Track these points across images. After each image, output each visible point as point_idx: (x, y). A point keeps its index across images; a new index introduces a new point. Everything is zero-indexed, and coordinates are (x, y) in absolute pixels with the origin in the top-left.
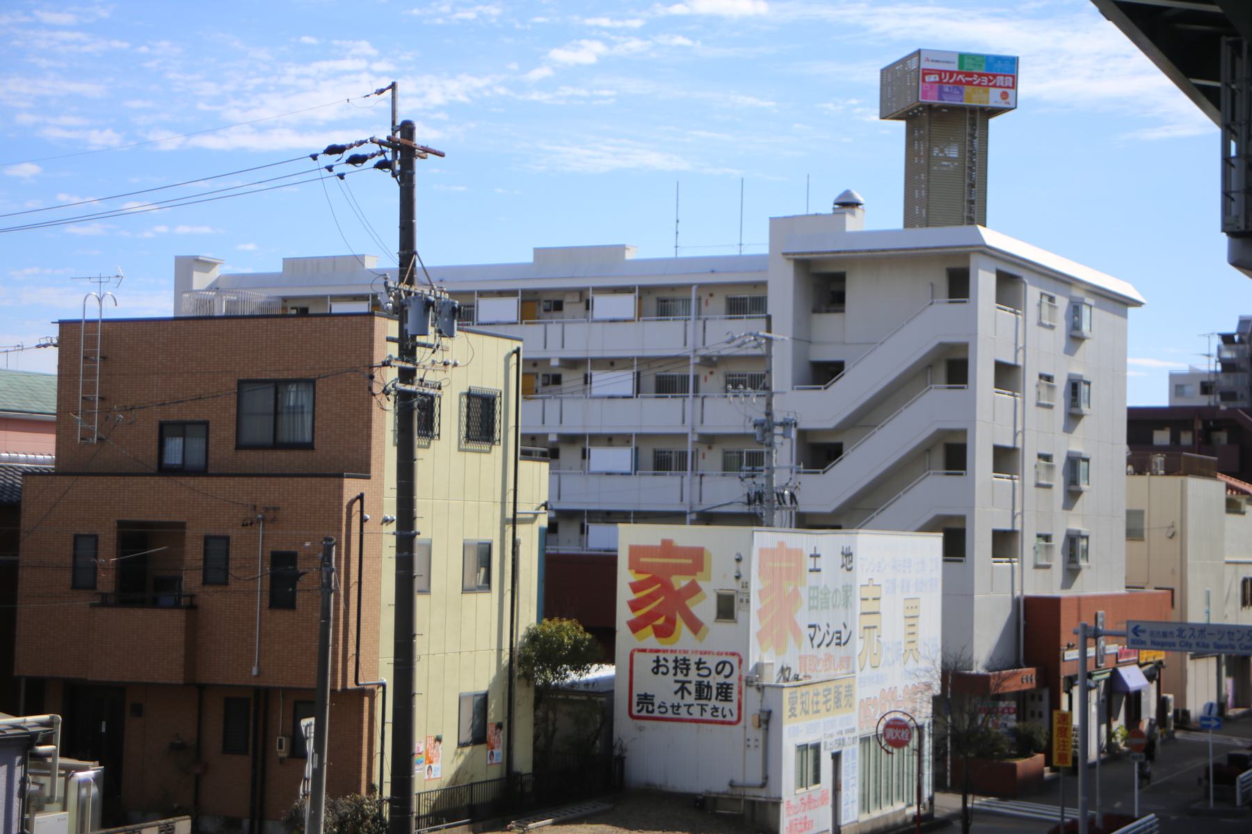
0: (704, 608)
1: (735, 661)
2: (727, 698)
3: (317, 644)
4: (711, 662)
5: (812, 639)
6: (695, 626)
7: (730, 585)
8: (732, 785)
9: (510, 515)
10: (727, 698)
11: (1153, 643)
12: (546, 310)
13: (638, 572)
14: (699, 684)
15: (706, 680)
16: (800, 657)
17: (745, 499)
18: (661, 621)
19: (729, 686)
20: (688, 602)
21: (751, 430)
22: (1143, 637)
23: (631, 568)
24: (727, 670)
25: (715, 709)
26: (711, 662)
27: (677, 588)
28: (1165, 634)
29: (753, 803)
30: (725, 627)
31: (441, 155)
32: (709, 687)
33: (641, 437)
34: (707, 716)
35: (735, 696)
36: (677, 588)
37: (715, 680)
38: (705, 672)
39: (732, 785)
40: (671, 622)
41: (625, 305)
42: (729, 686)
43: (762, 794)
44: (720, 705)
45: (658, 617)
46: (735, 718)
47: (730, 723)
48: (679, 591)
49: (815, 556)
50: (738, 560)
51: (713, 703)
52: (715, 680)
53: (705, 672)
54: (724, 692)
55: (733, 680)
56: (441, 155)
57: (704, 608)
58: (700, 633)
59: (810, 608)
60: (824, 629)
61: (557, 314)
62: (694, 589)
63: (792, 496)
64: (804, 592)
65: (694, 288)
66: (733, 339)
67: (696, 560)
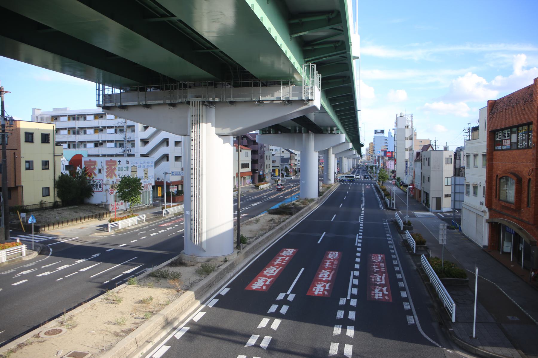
0: (96, 171)
1: (101, 180)
2: (101, 187)
3: (516, 173)
4: (98, 181)
5: (119, 176)
6: (95, 174)
7: (100, 167)
8: (102, 202)
9: (395, 147)
10: (101, 187)
11: (175, 175)
12: (100, 117)
13: (107, 166)
14: (96, 185)
15: (97, 184)
16: (116, 180)
17: (122, 152)
18: (89, 174)
19: (101, 185)
20: (94, 170)
21: (123, 139)
22: (174, 174)
23: (106, 165)
24: (100, 183)
25: (99, 189)
26: (98, 181)
27: (92, 168)
28: (177, 173)
29: (105, 205)
30: (100, 174)
31: (10, 92)
32: (98, 185)
33: (116, 141)
34: (97, 190)
35: (102, 187)
36: (92, 168)
37: (98, 184)
38: (97, 183)
39: (102, 202)
40: (91, 174)
41: (66, 118)
42: (101, 185)
43: (107, 203)
44: (99, 188)
45: (89, 173)
46: (102, 190)
47: (101, 191)
48: (92, 168)
49: (119, 162)
50: (102, 163)
51: (98, 188)
52: (98, 184)
53: (97, 183)
54: (100, 186)
55: (101, 184)
56: (10, 92)
57: (96, 171)
58: (96, 176)
59: (118, 171)
60: (122, 174)
61: (102, 118)
62: (95, 168)
63: (130, 151)
64: (117, 168)
65: (76, 115)
66: (119, 123)
67: (95, 163)
